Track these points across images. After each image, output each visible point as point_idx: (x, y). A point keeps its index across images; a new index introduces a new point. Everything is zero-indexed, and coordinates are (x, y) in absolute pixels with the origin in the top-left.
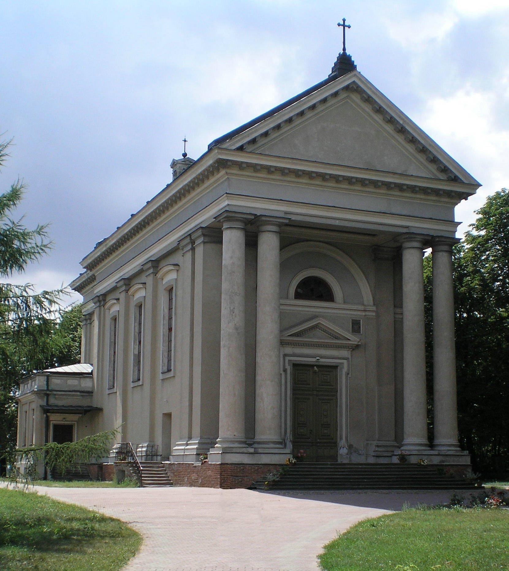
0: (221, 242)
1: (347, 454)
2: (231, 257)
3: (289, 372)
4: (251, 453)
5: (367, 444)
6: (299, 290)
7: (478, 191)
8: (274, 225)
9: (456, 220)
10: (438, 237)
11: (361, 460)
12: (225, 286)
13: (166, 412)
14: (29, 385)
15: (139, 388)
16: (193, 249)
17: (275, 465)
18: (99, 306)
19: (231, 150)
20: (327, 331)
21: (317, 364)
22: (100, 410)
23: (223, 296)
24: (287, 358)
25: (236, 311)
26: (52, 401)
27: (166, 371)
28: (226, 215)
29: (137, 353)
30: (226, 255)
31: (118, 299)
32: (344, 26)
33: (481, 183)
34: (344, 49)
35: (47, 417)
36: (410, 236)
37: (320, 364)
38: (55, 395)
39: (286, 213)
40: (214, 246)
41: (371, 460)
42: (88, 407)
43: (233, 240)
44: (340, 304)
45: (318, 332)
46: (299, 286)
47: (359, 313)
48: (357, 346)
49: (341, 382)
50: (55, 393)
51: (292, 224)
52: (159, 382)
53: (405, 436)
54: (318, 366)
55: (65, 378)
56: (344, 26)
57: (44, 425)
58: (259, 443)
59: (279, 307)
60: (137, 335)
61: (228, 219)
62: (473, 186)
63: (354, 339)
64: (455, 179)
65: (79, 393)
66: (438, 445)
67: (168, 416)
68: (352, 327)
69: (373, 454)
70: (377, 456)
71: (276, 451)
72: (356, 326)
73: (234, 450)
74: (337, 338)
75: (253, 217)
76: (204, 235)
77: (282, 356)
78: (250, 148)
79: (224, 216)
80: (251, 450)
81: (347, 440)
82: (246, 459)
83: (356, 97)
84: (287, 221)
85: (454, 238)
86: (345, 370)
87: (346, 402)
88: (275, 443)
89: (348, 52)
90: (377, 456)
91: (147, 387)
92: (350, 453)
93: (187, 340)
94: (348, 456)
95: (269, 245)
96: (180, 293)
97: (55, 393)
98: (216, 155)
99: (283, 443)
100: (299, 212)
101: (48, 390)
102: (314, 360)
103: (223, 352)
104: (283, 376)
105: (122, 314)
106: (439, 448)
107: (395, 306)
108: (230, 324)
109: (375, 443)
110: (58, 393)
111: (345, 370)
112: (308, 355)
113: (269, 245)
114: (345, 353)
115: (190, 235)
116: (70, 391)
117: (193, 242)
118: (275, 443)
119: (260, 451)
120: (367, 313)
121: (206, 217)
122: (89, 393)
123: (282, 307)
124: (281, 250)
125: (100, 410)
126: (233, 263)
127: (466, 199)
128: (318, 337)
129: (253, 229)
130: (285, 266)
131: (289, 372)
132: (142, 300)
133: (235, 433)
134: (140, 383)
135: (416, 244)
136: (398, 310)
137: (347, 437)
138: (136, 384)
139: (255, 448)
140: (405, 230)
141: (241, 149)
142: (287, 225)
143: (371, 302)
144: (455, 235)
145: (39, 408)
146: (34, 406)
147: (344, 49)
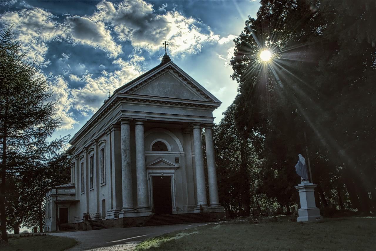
0: (121, 130)
1: (176, 211)
2: (124, 135)
3: (151, 179)
4: (136, 213)
5: (184, 207)
6: (154, 147)
7: (221, 105)
8: (141, 122)
9: (214, 116)
10: (207, 123)
11: (182, 213)
12: (123, 147)
13: (103, 199)
14: (49, 193)
15: (93, 191)
16: (110, 133)
17: (146, 216)
18: (77, 159)
19: (122, 93)
20: (165, 163)
21: (162, 176)
22: (79, 201)
23: (122, 151)
24: (150, 174)
25: (127, 156)
26: (59, 199)
27: (103, 182)
28: (121, 119)
29: (91, 177)
30: (122, 135)
31: (84, 156)
32: (165, 44)
33: (222, 102)
34: (166, 53)
35: (57, 205)
36: (196, 124)
37: (163, 176)
38: (60, 196)
39: (146, 117)
40: (118, 131)
41: (187, 212)
42: (74, 200)
43: (125, 128)
44: (170, 152)
45: (162, 163)
46: (153, 146)
47: (179, 155)
48: (178, 168)
49: (172, 182)
50: (60, 195)
51: (148, 121)
52: (100, 187)
53: (198, 202)
54: (162, 177)
55: (64, 189)
56: (165, 44)
57: (56, 209)
58: (139, 208)
59: (145, 154)
60: (91, 170)
61: (123, 120)
62: (219, 104)
63: (176, 165)
64: (211, 101)
65: (69, 195)
66: (211, 205)
67: (104, 201)
68: (176, 161)
69: (187, 210)
70: (188, 211)
71: (146, 211)
72: (177, 160)
73: (129, 212)
74: (170, 165)
75: (132, 119)
76: (114, 127)
77: (148, 174)
78: (131, 92)
79: (121, 119)
80: (136, 211)
81: (176, 205)
82: (134, 215)
83: (171, 71)
84: (146, 120)
85: (213, 124)
86: (173, 178)
87: (175, 190)
88: (145, 208)
89: (167, 54)
90: (188, 211)
91: (96, 189)
92: (177, 211)
93: (110, 170)
94: (177, 212)
95: (139, 130)
96: (106, 151)
97: (60, 195)
98: (116, 96)
99: (148, 208)
100: (151, 117)
101: (57, 194)
102: (161, 174)
103: (123, 173)
104: (149, 182)
105: (85, 161)
106: (212, 206)
107: (192, 152)
108: (125, 162)
109: (187, 206)
110: (61, 195)
111: (173, 178)
112: (158, 173)
113: (139, 130)
114: (173, 171)
115: (109, 128)
116: (66, 194)
117: (110, 130)
118: (145, 208)
119: (139, 211)
120: (181, 155)
121: (114, 121)
122: (74, 195)
123: (146, 154)
124: (144, 132)
125: (79, 201)
126: (125, 138)
127: (217, 108)
128: (162, 165)
129: (132, 123)
130: (146, 139)
131: (151, 179)
132: (93, 155)
133: (129, 205)
134: (93, 189)
135: (198, 127)
136: (194, 153)
137: (175, 204)
138: (92, 189)
139: (137, 210)
140: (194, 122)
141: (126, 93)
142: (146, 121)
143: (183, 151)
144: (213, 122)
145: (53, 202)
146: (51, 201)
147: (166, 53)
